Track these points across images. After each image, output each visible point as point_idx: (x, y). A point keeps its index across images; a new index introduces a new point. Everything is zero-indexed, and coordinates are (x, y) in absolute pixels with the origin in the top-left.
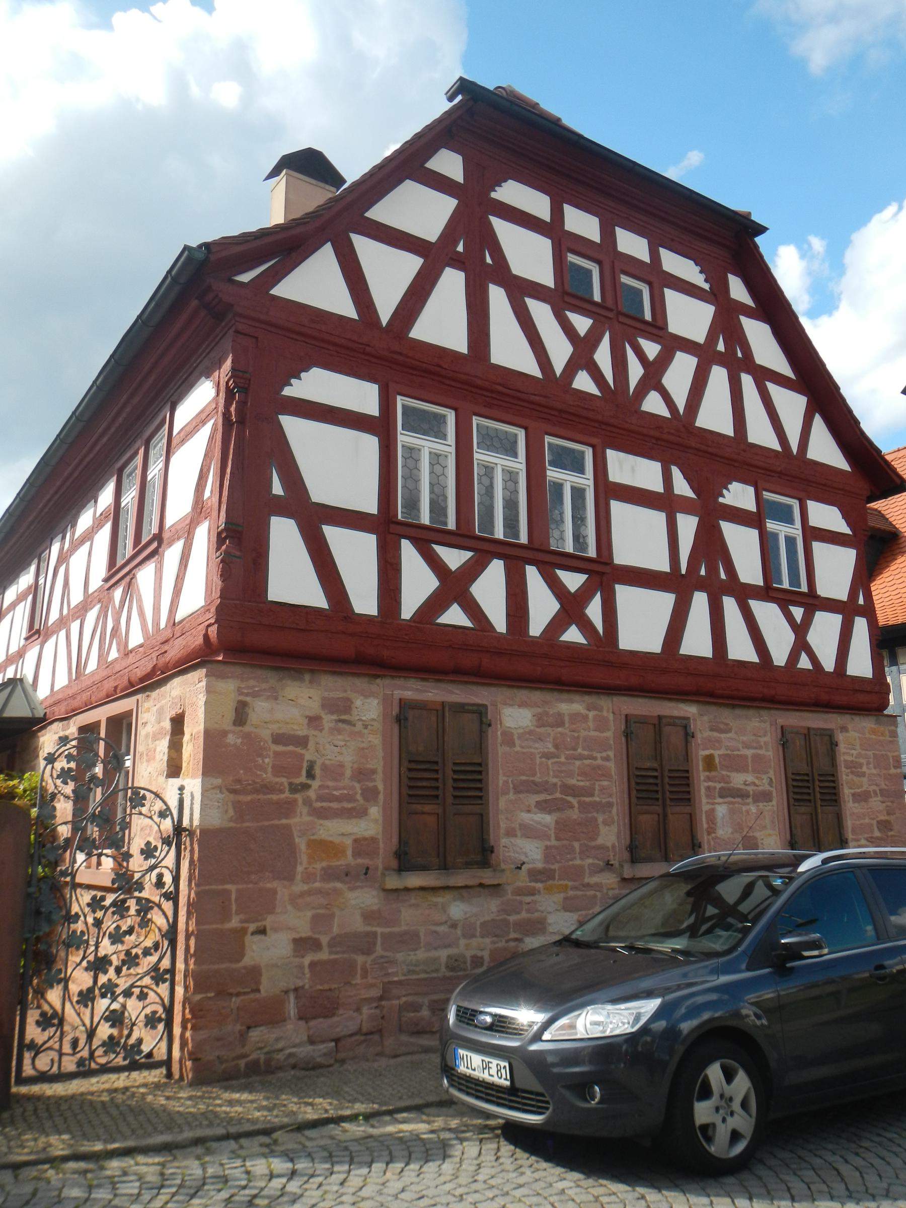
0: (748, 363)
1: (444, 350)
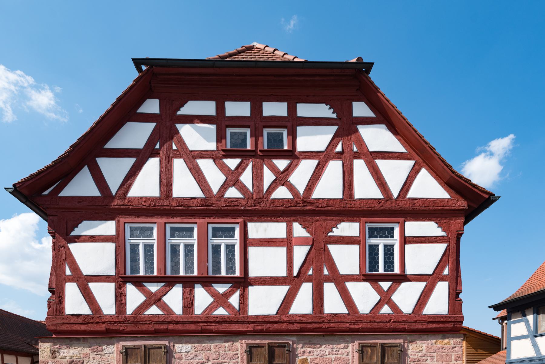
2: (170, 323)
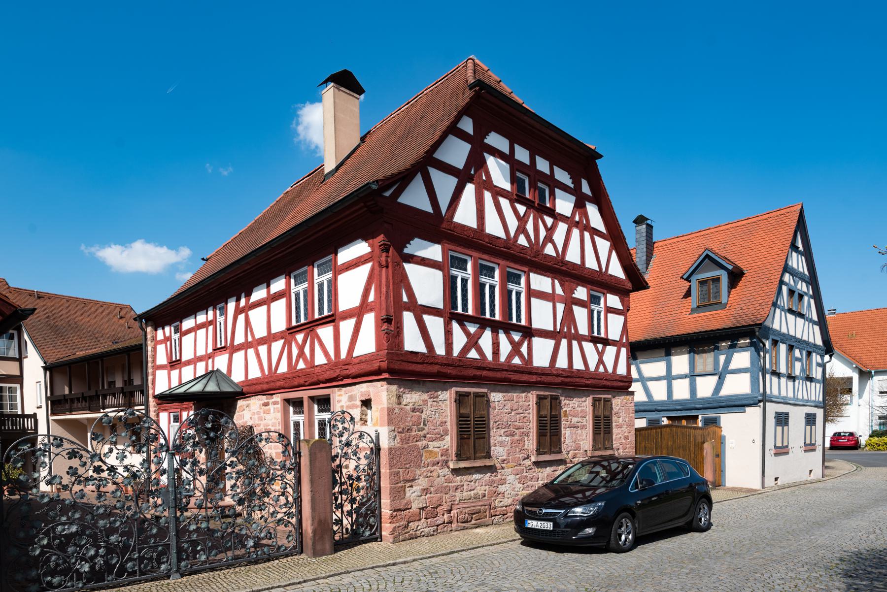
0: (488, 184)
1: (464, 226)
2: (484, 369)
